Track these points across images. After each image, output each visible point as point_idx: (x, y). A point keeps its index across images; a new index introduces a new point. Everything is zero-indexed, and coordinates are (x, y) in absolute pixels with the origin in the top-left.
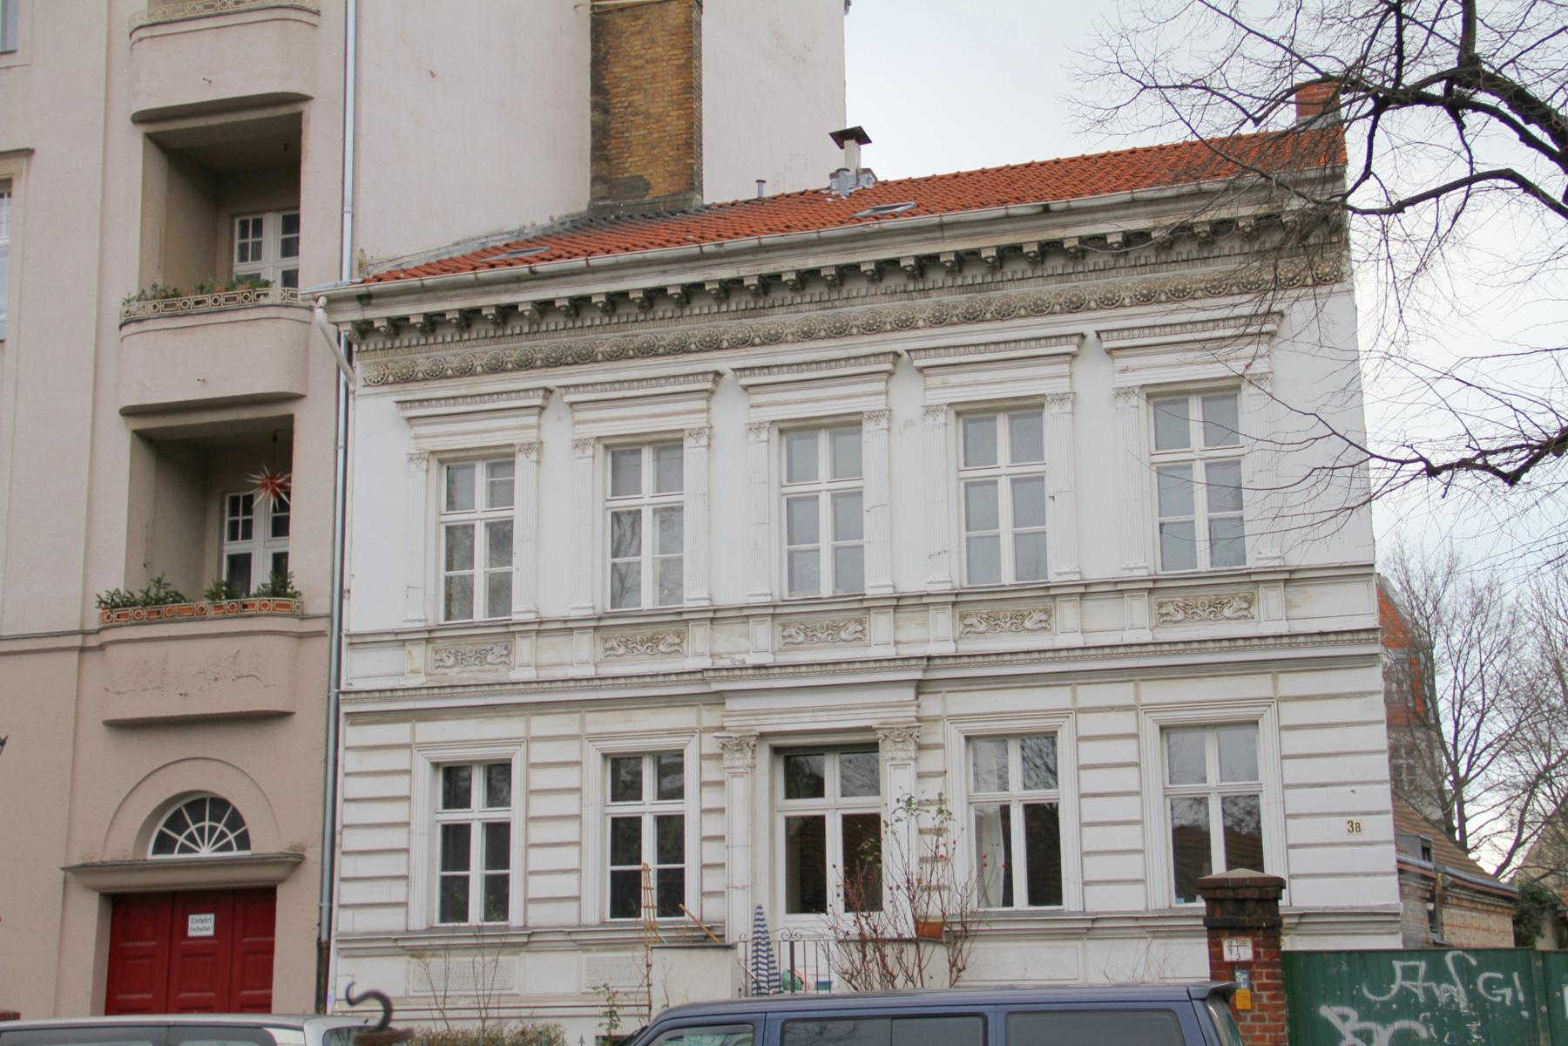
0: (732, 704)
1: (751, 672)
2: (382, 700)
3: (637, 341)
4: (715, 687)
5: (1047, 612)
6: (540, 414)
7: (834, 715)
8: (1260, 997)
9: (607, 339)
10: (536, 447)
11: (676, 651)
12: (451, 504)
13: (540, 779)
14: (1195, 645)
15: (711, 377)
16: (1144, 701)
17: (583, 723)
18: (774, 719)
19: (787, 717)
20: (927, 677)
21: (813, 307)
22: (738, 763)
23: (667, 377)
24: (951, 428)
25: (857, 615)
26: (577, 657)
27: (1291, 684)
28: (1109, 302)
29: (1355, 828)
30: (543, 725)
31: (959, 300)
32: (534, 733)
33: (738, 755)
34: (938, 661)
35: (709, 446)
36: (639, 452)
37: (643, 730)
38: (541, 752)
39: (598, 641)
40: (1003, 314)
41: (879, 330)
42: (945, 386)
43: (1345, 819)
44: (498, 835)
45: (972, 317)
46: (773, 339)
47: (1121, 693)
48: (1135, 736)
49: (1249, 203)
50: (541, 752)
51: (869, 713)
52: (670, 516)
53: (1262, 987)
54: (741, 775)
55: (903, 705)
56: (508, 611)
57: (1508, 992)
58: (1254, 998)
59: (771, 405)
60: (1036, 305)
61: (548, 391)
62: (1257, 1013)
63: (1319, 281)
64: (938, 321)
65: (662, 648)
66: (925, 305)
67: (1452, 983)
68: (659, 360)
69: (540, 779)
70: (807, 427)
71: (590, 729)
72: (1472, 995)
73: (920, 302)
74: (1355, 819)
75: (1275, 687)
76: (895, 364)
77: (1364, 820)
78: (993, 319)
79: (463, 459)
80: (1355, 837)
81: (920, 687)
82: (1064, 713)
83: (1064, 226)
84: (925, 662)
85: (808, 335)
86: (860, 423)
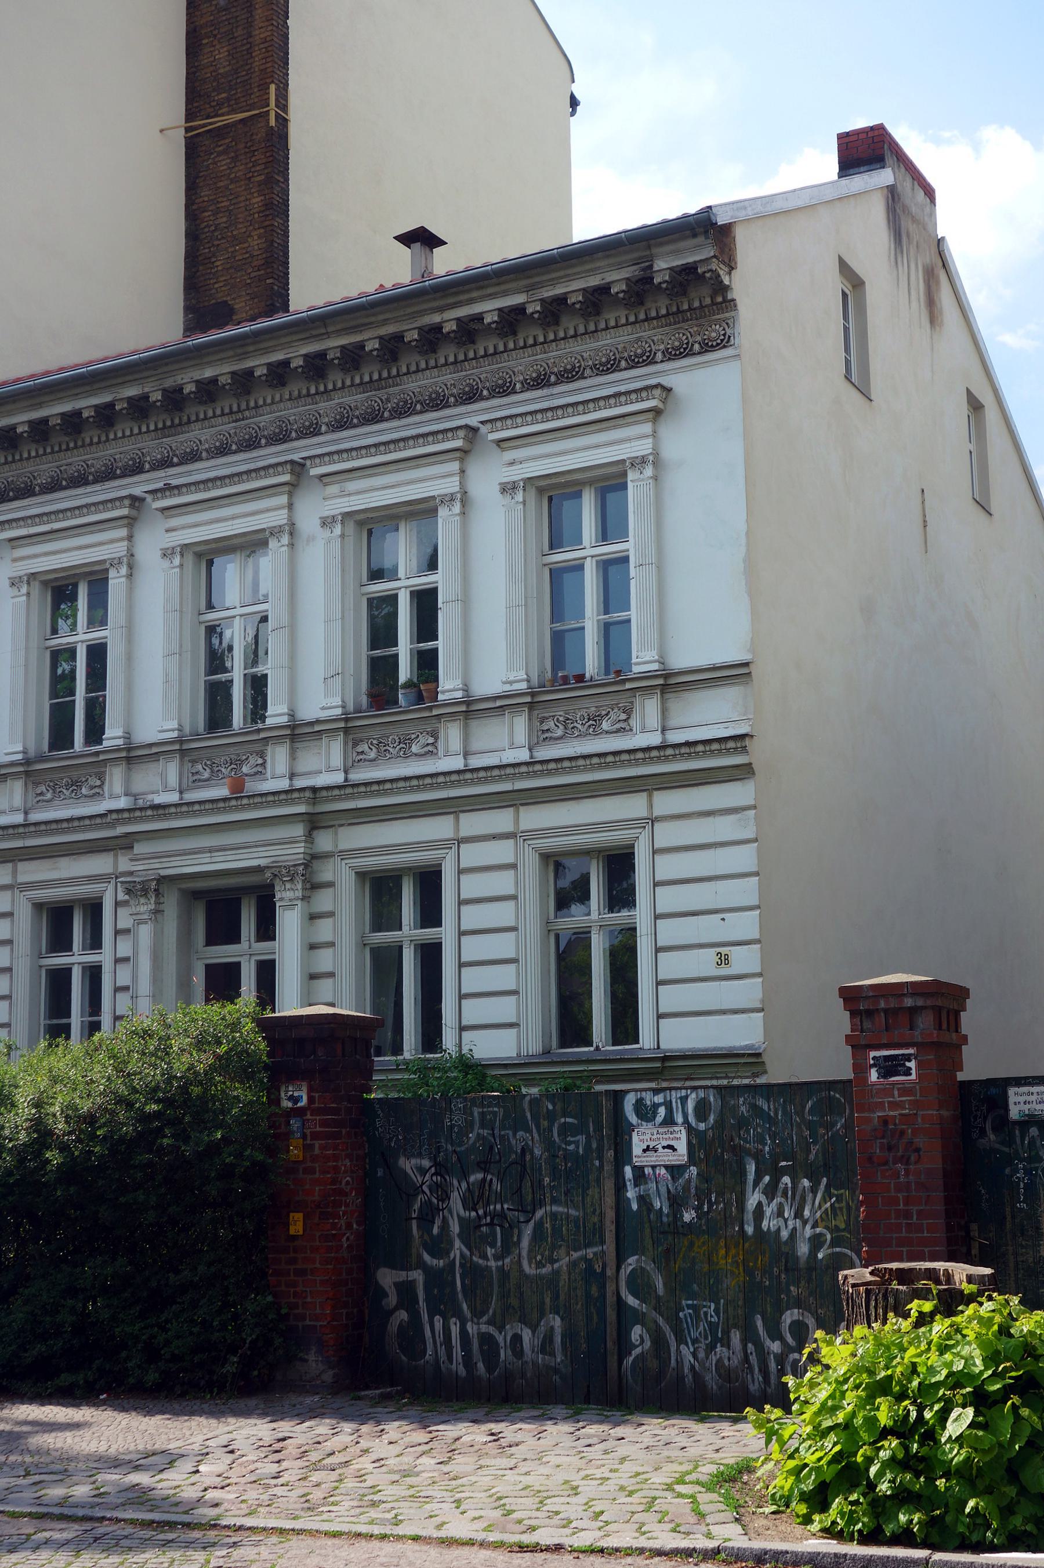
0: (139, 848)
1: (149, 812)
2: (600, 767)
3: (71, 470)
4: (121, 830)
5: (262, 754)
6: (655, 421)
7: (230, 855)
8: (312, 1146)
9: (45, 469)
10: (131, 562)
11: (97, 795)
12: (555, 543)
13: (472, 886)
14: (566, 764)
15: (127, 502)
16: (522, 827)
17: (15, 873)
18: (176, 861)
19: (188, 860)
20: (318, 811)
21: (226, 419)
22: (143, 909)
23: (339, 452)
24: (350, 541)
25: (257, 747)
26: (505, 742)
27: (667, 802)
28: (504, 389)
29: (724, 960)
30: (473, 823)
31: (356, 399)
32: (463, 833)
33: (142, 900)
34: (324, 793)
35: (655, 478)
36: (578, 495)
37: (68, 876)
38: (471, 856)
39: (30, 786)
40: (403, 410)
41: (317, 433)
42: (343, 494)
43: (713, 951)
44: (430, 956)
45: (373, 417)
46: (193, 457)
47: (501, 820)
48: (513, 866)
49: (620, 267)
50: (471, 856)
51: (263, 852)
52: (614, 568)
53: (315, 1136)
54: (146, 923)
55: (292, 841)
56: (263, 718)
57: (582, 1138)
58: (307, 1148)
59: (183, 527)
60: (431, 399)
61: (136, 501)
62: (309, 1164)
63: (708, 347)
64: (341, 424)
65: (84, 791)
66: (327, 408)
67: (528, 1130)
68: (89, 489)
69: (472, 886)
70: (227, 546)
71: (22, 878)
72: (549, 1145)
73: (323, 406)
74: (724, 950)
75: (651, 806)
76: (664, 401)
77: (734, 952)
78: (391, 418)
79: (567, 484)
80: (724, 971)
81: (314, 823)
82: (445, 844)
83: (441, 309)
84: (308, 794)
85: (223, 450)
86: (435, 511)
